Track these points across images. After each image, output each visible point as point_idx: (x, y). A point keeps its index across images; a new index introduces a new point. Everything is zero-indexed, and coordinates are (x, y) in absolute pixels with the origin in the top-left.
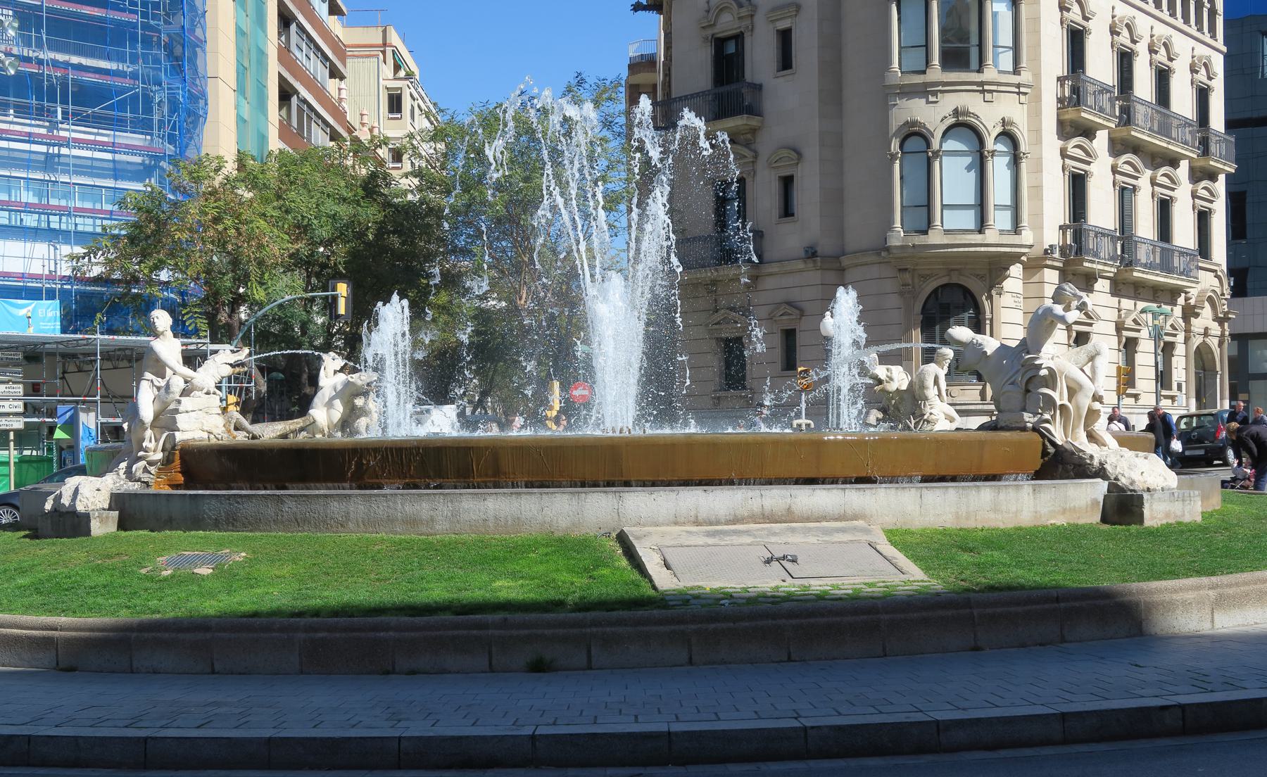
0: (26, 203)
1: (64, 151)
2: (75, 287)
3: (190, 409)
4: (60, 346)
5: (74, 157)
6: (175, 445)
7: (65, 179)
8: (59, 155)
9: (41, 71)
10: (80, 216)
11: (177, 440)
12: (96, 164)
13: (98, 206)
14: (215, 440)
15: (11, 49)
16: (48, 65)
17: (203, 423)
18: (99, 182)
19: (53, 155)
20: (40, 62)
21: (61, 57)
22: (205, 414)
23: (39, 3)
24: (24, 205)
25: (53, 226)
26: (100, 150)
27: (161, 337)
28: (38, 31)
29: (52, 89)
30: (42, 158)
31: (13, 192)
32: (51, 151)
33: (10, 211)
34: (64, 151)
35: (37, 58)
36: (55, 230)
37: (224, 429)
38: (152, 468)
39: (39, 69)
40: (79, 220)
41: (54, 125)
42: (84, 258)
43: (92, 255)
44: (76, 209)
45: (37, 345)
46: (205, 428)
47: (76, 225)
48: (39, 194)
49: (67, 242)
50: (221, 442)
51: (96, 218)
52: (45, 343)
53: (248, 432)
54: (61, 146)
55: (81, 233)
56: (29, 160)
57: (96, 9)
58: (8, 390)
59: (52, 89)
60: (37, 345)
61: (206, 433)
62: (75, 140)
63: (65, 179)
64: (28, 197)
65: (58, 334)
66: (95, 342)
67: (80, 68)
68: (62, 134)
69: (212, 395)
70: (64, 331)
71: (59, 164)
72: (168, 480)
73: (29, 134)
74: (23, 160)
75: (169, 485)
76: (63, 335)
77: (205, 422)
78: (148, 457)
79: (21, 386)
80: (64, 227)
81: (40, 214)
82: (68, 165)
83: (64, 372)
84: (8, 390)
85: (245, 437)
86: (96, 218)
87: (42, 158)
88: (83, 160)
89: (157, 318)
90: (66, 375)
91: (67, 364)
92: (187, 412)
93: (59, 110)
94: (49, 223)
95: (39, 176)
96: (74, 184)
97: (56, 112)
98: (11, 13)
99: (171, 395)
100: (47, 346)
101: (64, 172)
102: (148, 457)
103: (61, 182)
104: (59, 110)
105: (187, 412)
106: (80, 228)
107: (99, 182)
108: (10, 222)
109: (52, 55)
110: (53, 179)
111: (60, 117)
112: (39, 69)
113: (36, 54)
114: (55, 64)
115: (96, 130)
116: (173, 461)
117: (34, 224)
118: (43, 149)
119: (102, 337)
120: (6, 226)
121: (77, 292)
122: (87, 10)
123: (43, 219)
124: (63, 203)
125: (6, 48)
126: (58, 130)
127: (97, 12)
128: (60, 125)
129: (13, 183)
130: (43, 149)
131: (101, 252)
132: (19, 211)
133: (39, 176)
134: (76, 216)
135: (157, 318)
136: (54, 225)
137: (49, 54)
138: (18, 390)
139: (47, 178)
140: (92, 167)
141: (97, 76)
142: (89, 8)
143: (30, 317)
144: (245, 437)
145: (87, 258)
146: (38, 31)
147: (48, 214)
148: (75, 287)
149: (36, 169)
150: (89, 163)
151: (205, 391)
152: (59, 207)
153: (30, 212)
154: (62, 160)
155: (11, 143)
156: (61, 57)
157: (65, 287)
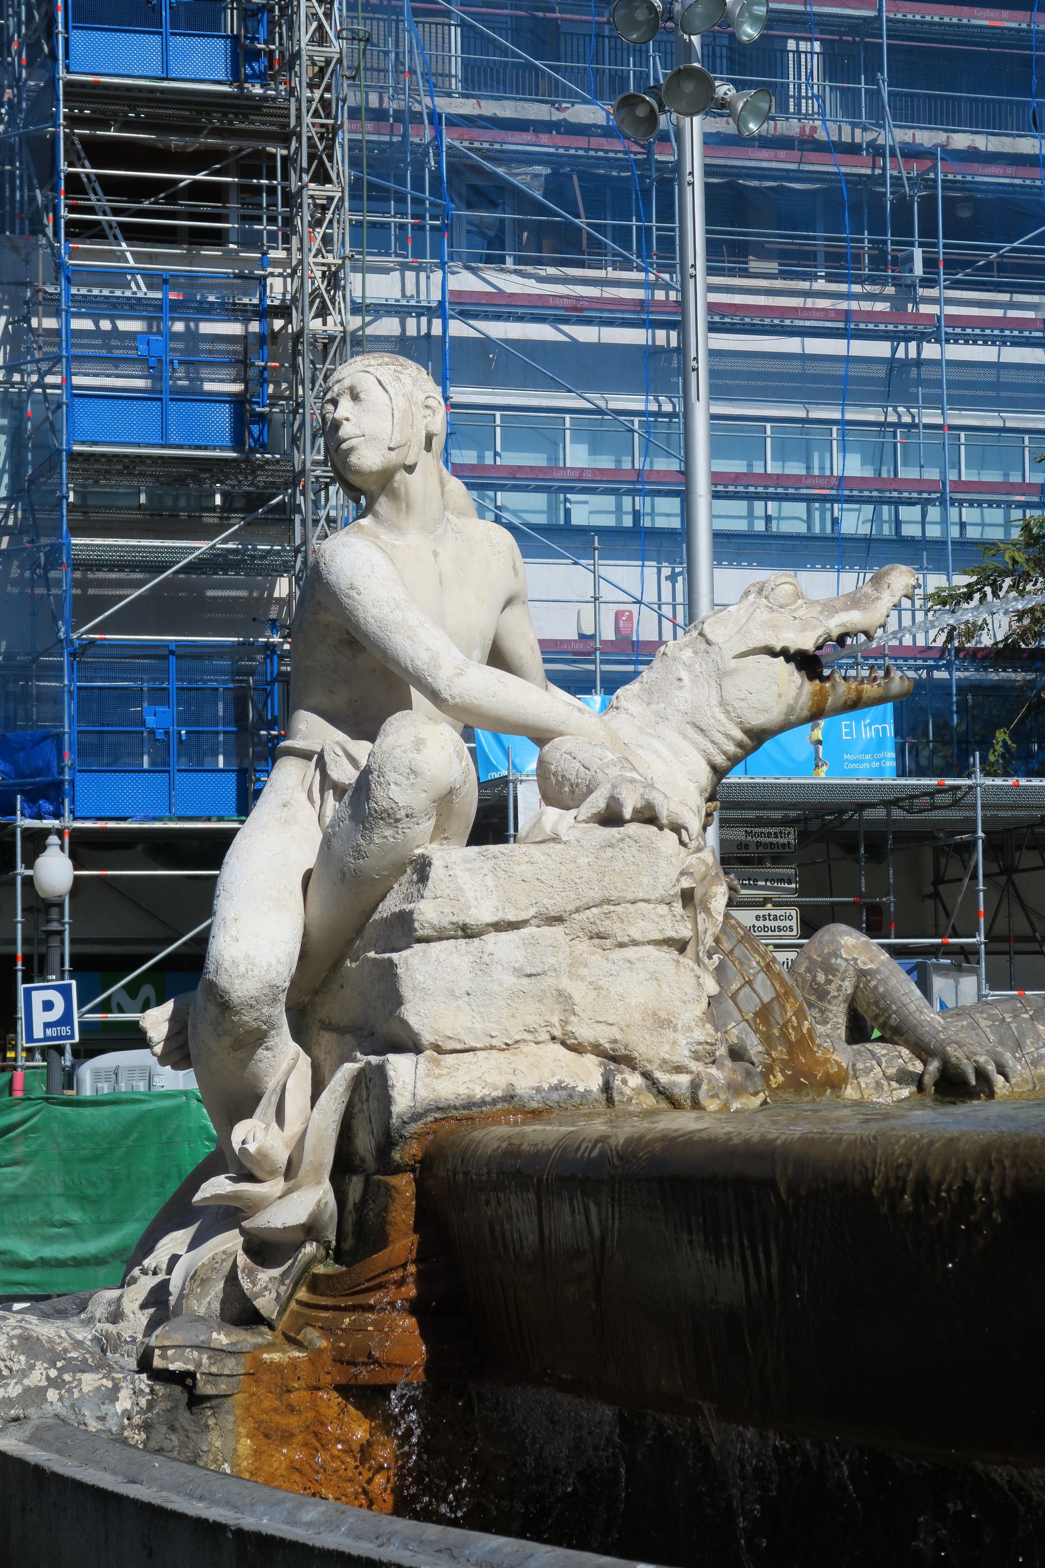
0: (841, 479)
1: (931, 351)
2: (957, 674)
3: (483, 913)
4: (897, 813)
5: (951, 363)
6: (388, 1141)
7: (931, 417)
8: (919, 363)
9: (878, 171)
10: (971, 503)
11: (402, 1103)
12: (1007, 377)
13: (1015, 478)
14: (649, 1101)
15: (814, 129)
16: (893, 155)
17: (564, 999)
18: (1015, 420)
19: (907, 363)
20: (877, 150)
21: (926, 138)
22: (583, 946)
23: (872, 13)
24: (834, 482)
25: (908, 531)
26: (1017, 343)
27: (383, 505)
28: (871, 80)
29: (903, 206)
30: (881, 372)
31: (816, 456)
32: (900, 354)
33: (809, 499)
34: (931, 351)
35: (872, 144)
36: (911, 541)
37: (703, 1033)
38: (265, 1275)
39: (874, 168)
40: (969, 514)
41: (907, 290)
42: (968, 597)
43: (988, 590)
44: (960, 486)
45: (842, 812)
46: (586, 1033)
47: (963, 525)
48: (876, 456)
49: (939, 566)
50: (685, 1122)
51: (1009, 505)
52: (862, 806)
53: (922, 1050)
54: (921, 337)
55: (974, 543)
56: (846, 379)
57: (1005, 14)
58: (761, 923)
59: (903, 206)
60: (842, 812)
61: (591, 1061)
62: (953, 321)
63: (931, 417)
64: (854, 466)
65: (890, 779)
66: (968, 800)
67: (972, 155)
68: (925, 309)
69: (633, 829)
70: (902, 773)
71: (919, 382)
72: (341, 1360)
73: (847, 315)
74: (833, 379)
75: (343, 1390)
76: (902, 781)
77: (577, 991)
78: (255, 1206)
79: (793, 912)
80: (934, 532)
81: (878, 502)
82: (938, 384)
83: (938, 881)
84: (761, 923)
85: (903, 1077)
86: (1009, 505)
87: (881, 372)
88: (976, 370)
89: (355, 397)
90: (941, 888)
91: (943, 861)
92: (467, 932)
93: (918, 253)
94: (898, 523)
95: (872, 415)
96: (952, 428)
97: (910, 259)
98: (817, 46)
99: (384, 835)
100: (869, 814)
101: (933, 402)
102: (255, 1206)
103: (927, 426)
104: (918, 253)
105: (467, 932)
106: (973, 533)
107: (1015, 420)
108: (809, 528)
109: (904, 136)
110: (906, 419)
111: (918, 269)
112: (874, 168)
113: (869, 136)
114: (911, 153)
115: (1005, 297)
116: (381, 1241)
117: (864, 530)
118: (881, 349)
119: (989, 781)
120: (797, 537)
121: (964, 688)
122: (983, 18)
123: (886, 517)
124: (932, 474)
125: (803, 129)
126: (916, 304)
127: (1008, 20)
128: (921, 292)
129: (816, 434)
130: (881, 349)
131: (1008, 581)
132: (823, 499)
133: (872, 415)
134: (961, 503)
135: (355, 397)
136: (911, 530)
137: (897, 132)
138: (788, 923)
139: (892, 418)
140: (997, 386)
141: (1010, 170)
142: (988, 12)
143: (819, 742)
144: (903, 1077)
145: (977, 596)
146: (871, 80)
147: (897, 503)
148: (957, 674)
149: (864, 399)
150: (990, 376)
151: (597, 802)
152: (920, 484)
153: (850, 500)
154: (926, 373)
155: (808, 341)
156: (926, 138)
157: (937, 675)
